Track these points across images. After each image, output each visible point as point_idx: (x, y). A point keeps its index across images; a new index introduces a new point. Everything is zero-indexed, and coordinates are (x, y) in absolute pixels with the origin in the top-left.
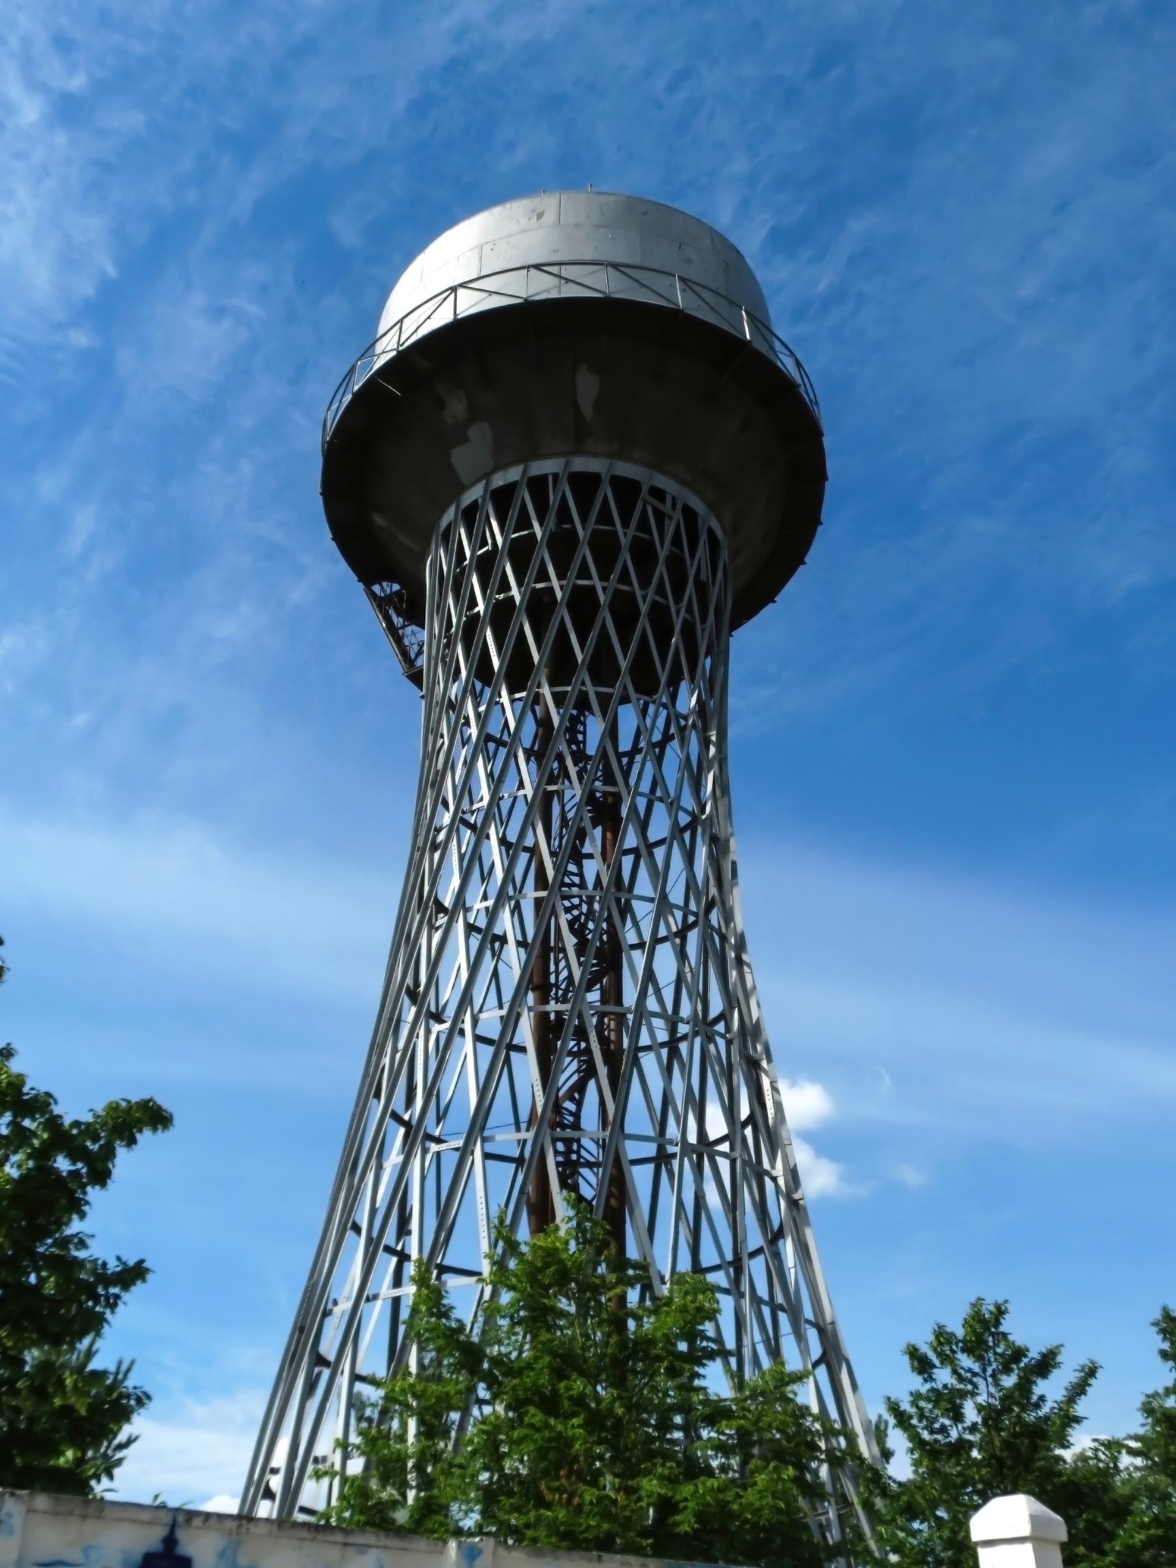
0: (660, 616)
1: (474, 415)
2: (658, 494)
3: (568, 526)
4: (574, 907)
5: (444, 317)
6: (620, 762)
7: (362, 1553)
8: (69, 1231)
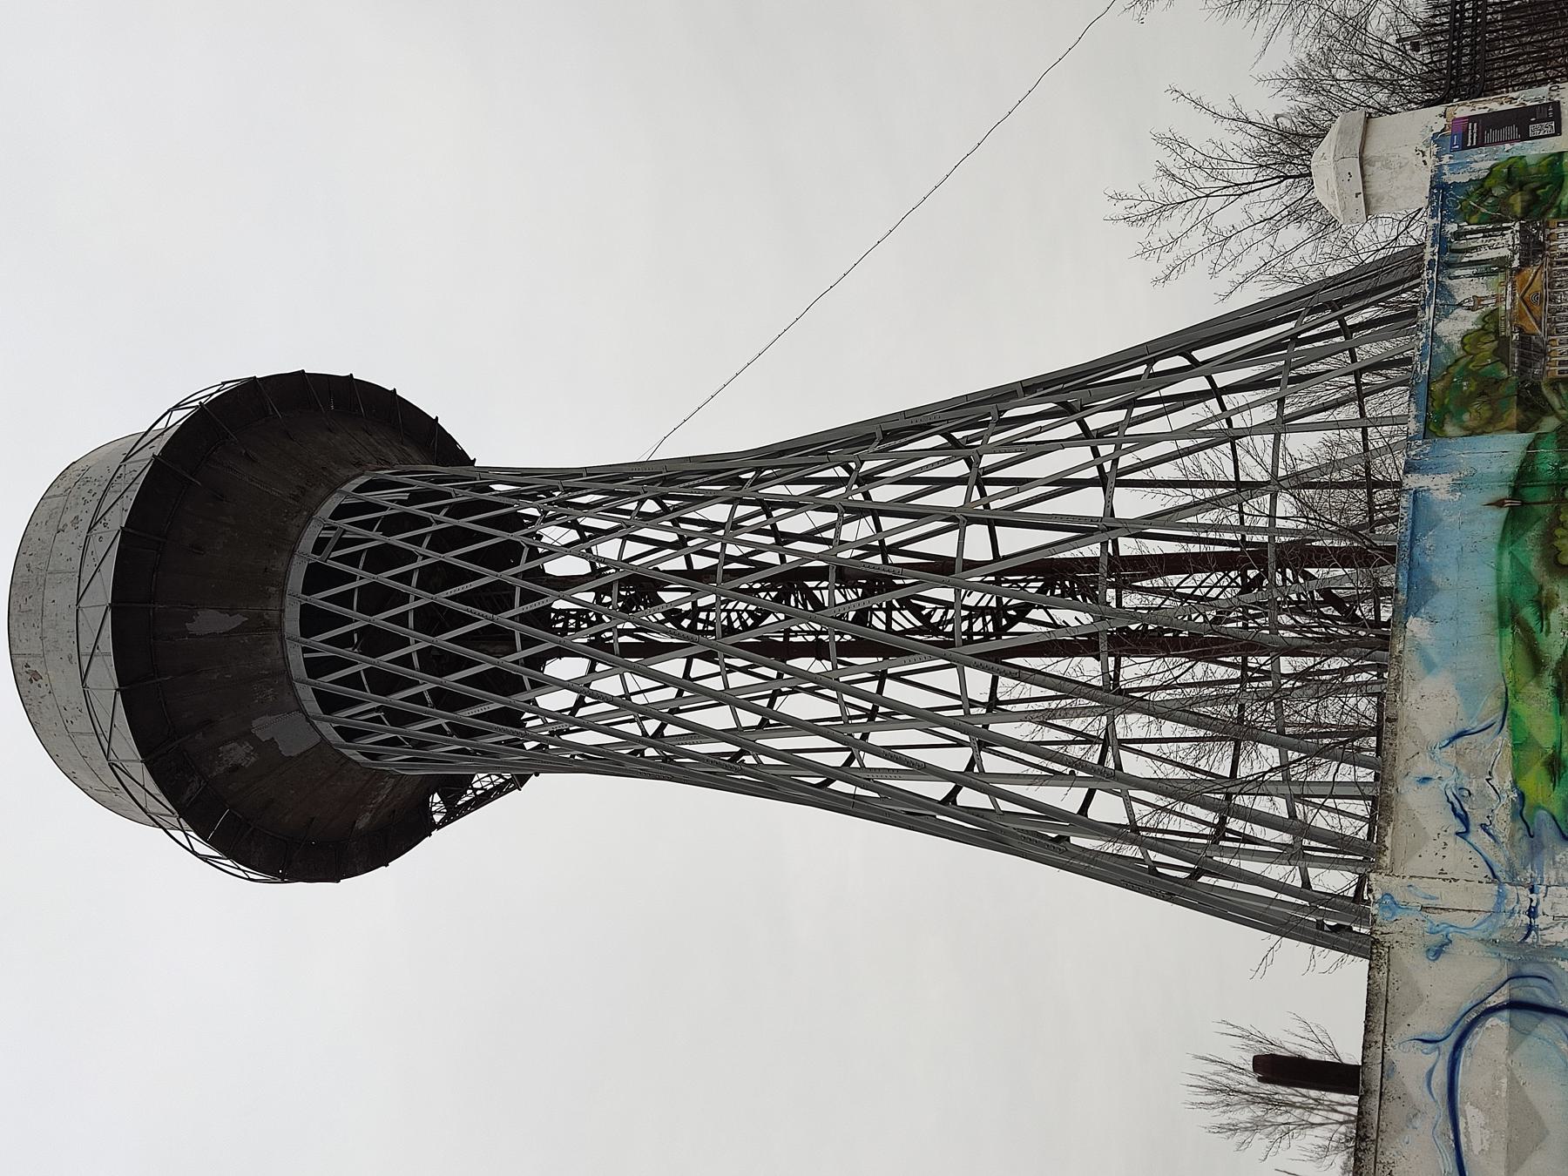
0: (444, 541)
1: (248, 736)
2: (320, 544)
5: (140, 771)
8: (1475, 315)
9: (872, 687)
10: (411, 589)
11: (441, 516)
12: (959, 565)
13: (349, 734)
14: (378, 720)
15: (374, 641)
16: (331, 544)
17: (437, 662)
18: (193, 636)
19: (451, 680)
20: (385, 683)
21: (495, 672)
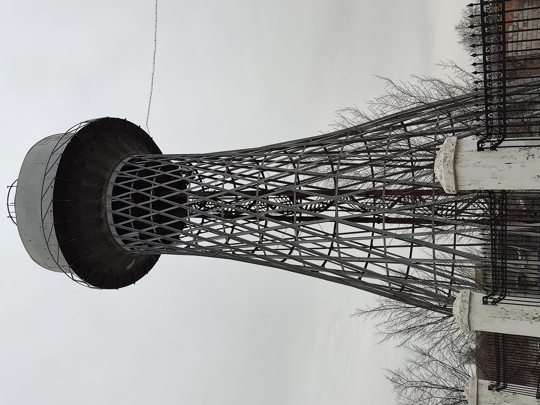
9: (372, 256)
11: (158, 171)
12: (384, 221)
13: (126, 242)
15: (137, 212)
17: (159, 219)
19: (164, 225)
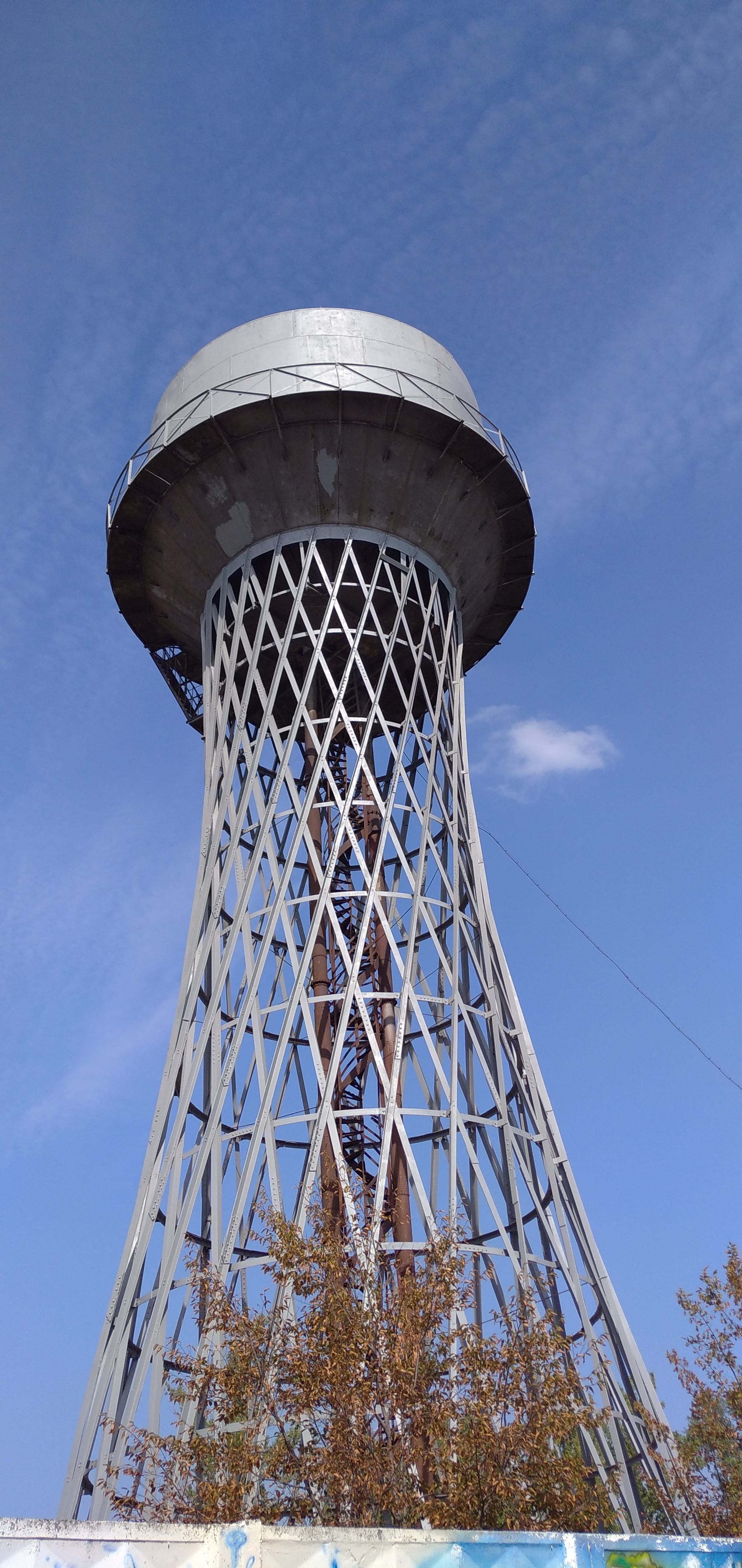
0: (402, 655)
1: (233, 499)
2: (394, 554)
3: (319, 585)
4: (346, 911)
6: (378, 785)
7: (111, 1550)
10: (361, 630)
14: (248, 603)
16: (395, 563)
18: (316, 455)
20: (281, 609)
21: (294, 703)
